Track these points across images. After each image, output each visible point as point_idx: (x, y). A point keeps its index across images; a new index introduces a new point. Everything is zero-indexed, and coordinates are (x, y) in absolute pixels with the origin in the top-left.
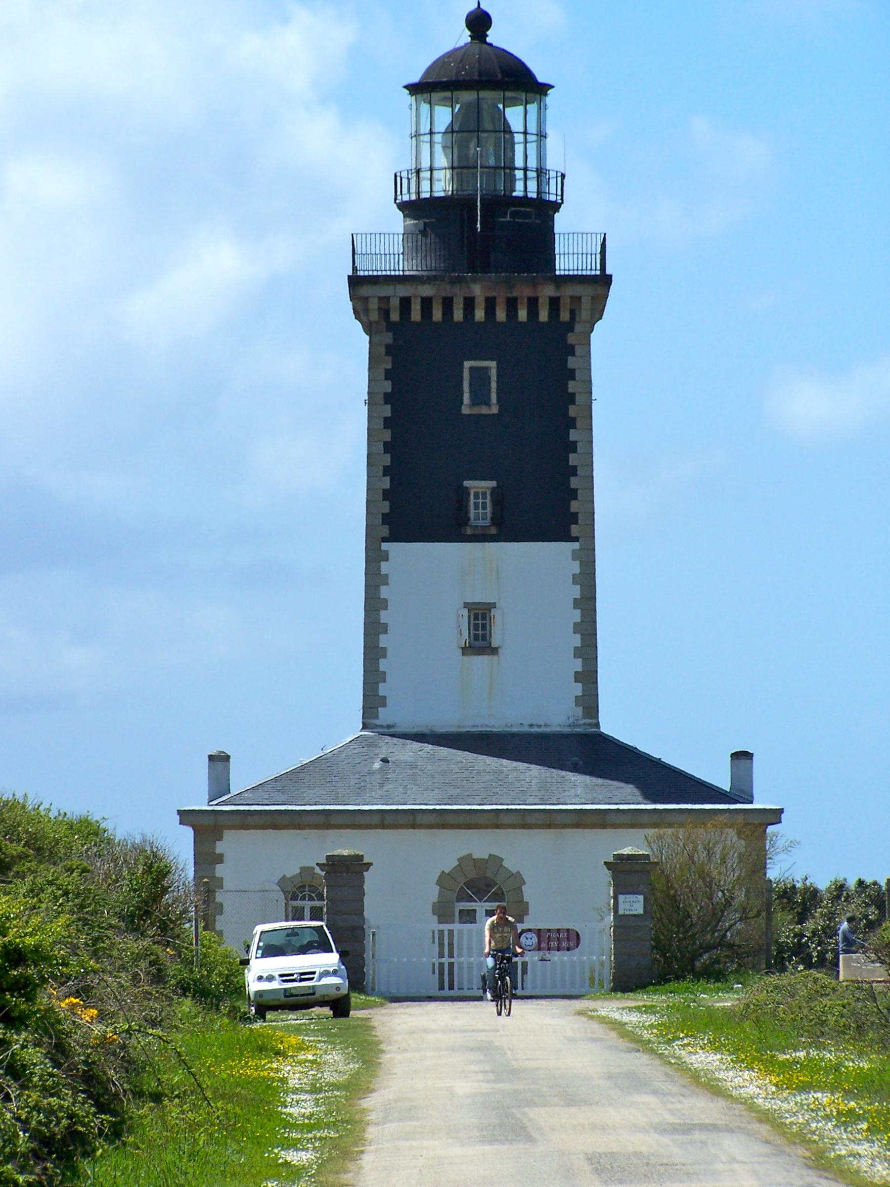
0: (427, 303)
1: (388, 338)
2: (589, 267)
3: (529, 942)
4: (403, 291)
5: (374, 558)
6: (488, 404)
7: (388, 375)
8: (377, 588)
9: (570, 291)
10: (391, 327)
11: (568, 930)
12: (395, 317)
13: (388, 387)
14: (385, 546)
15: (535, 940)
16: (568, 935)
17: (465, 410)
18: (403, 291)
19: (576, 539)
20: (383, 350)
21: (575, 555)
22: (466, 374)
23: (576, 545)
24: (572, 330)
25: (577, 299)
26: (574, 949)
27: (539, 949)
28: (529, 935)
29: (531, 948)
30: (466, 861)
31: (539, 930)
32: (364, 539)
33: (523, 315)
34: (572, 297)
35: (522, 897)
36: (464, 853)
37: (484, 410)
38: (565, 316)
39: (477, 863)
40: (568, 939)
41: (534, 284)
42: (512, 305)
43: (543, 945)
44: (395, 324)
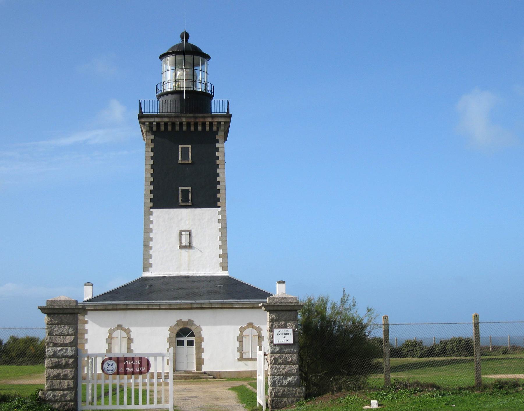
0: (166, 124)
1: (152, 137)
2: (224, 111)
3: (110, 368)
4: (157, 120)
5: (148, 214)
6: (188, 160)
7: (152, 150)
8: (148, 225)
9: (217, 120)
10: (153, 133)
11: (141, 358)
12: (155, 129)
13: (152, 154)
14: (152, 210)
15: (115, 366)
16: (141, 362)
17: (180, 162)
18: (157, 120)
19: (219, 207)
20: (150, 141)
21: (219, 213)
22: (180, 150)
23: (219, 209)
24: (218, 134)
25: (219, 123)
26: (145, 373)
27: (118, 373)
28: (110, 362)
29: (113, 372)
30: (179, 322)
31: (118, 358)
32: (253, 285)
33: (200, 128)
34: (217, 122)
35: (201, 335)
36: (179, 319)
37: (187, 162)
38: (215, 128)
39: (184, 322)
40: (141, 366)
41: (204, 117)
42: (196, 125)
43: (121, 370)
44: (155, 132)
